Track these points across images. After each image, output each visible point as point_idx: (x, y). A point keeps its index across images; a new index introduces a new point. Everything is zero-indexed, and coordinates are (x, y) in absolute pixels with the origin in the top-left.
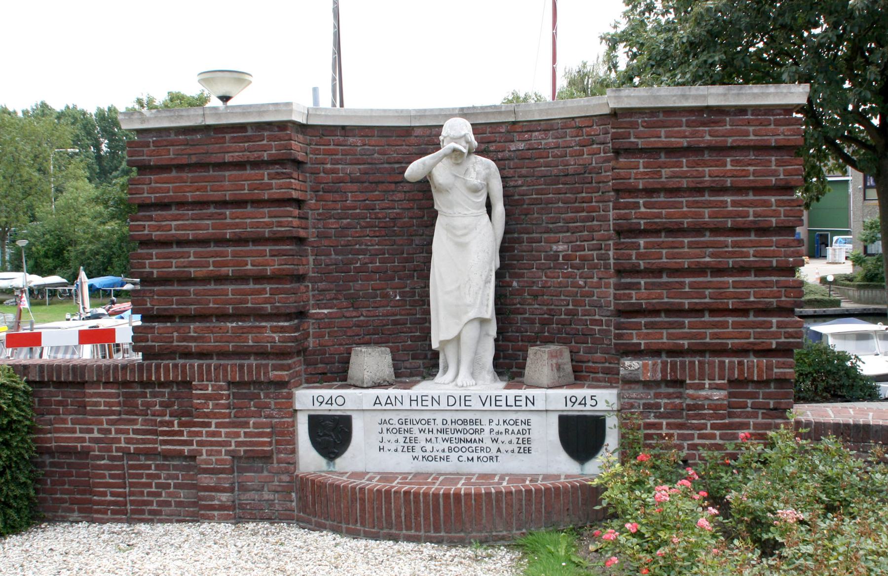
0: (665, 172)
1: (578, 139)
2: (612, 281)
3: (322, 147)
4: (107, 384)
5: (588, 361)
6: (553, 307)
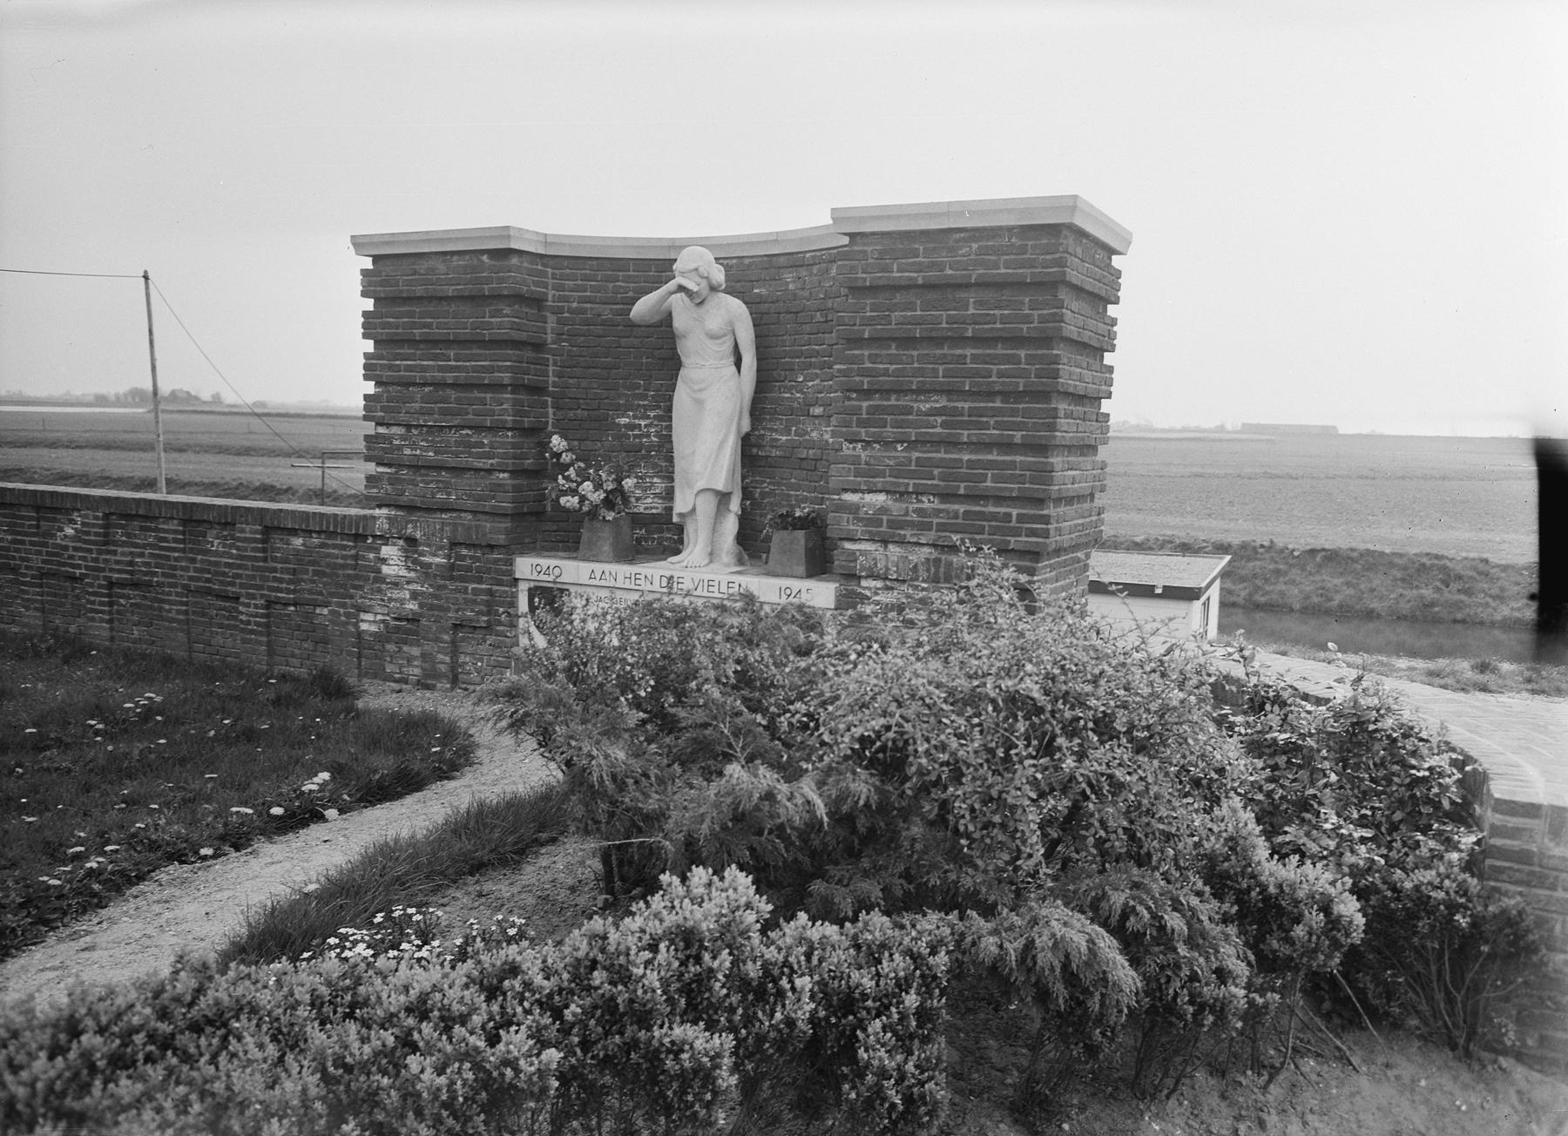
0: (896, 315)
4: (344, 535)
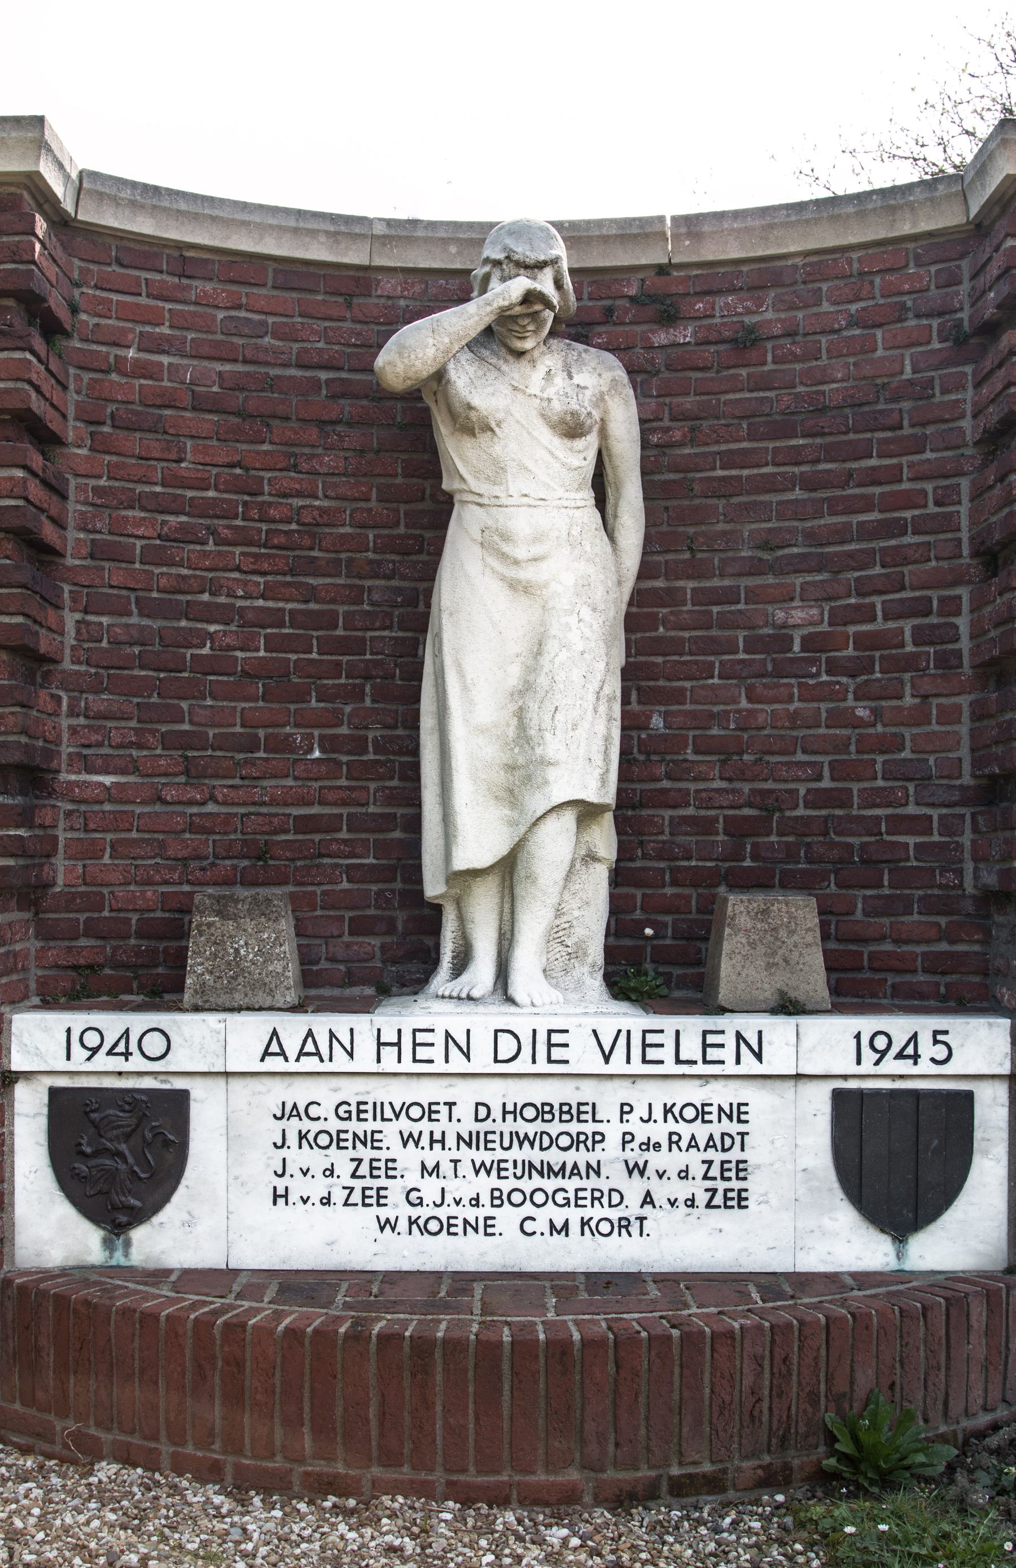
1: (854, 308)
2: (964, 701)
3: (115, 297)
5: (882, 938)
6: (769, 785)
